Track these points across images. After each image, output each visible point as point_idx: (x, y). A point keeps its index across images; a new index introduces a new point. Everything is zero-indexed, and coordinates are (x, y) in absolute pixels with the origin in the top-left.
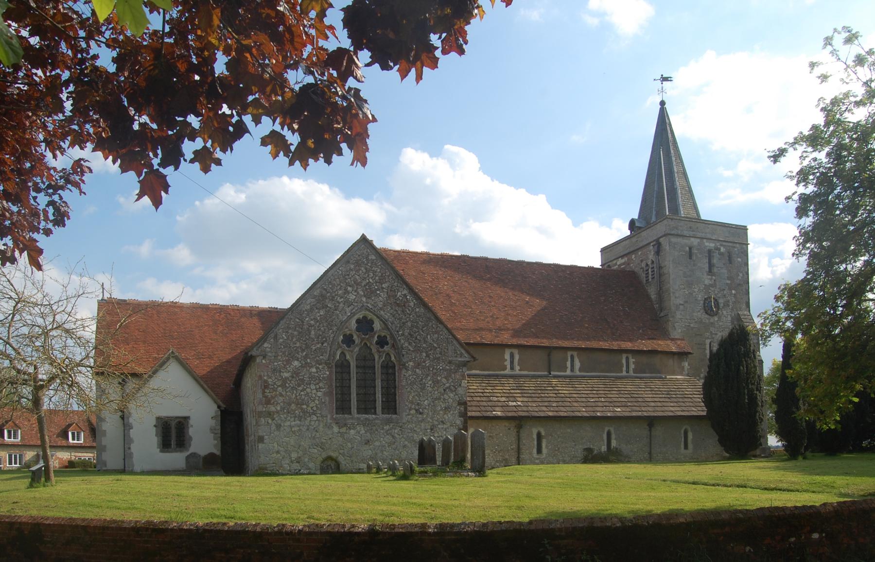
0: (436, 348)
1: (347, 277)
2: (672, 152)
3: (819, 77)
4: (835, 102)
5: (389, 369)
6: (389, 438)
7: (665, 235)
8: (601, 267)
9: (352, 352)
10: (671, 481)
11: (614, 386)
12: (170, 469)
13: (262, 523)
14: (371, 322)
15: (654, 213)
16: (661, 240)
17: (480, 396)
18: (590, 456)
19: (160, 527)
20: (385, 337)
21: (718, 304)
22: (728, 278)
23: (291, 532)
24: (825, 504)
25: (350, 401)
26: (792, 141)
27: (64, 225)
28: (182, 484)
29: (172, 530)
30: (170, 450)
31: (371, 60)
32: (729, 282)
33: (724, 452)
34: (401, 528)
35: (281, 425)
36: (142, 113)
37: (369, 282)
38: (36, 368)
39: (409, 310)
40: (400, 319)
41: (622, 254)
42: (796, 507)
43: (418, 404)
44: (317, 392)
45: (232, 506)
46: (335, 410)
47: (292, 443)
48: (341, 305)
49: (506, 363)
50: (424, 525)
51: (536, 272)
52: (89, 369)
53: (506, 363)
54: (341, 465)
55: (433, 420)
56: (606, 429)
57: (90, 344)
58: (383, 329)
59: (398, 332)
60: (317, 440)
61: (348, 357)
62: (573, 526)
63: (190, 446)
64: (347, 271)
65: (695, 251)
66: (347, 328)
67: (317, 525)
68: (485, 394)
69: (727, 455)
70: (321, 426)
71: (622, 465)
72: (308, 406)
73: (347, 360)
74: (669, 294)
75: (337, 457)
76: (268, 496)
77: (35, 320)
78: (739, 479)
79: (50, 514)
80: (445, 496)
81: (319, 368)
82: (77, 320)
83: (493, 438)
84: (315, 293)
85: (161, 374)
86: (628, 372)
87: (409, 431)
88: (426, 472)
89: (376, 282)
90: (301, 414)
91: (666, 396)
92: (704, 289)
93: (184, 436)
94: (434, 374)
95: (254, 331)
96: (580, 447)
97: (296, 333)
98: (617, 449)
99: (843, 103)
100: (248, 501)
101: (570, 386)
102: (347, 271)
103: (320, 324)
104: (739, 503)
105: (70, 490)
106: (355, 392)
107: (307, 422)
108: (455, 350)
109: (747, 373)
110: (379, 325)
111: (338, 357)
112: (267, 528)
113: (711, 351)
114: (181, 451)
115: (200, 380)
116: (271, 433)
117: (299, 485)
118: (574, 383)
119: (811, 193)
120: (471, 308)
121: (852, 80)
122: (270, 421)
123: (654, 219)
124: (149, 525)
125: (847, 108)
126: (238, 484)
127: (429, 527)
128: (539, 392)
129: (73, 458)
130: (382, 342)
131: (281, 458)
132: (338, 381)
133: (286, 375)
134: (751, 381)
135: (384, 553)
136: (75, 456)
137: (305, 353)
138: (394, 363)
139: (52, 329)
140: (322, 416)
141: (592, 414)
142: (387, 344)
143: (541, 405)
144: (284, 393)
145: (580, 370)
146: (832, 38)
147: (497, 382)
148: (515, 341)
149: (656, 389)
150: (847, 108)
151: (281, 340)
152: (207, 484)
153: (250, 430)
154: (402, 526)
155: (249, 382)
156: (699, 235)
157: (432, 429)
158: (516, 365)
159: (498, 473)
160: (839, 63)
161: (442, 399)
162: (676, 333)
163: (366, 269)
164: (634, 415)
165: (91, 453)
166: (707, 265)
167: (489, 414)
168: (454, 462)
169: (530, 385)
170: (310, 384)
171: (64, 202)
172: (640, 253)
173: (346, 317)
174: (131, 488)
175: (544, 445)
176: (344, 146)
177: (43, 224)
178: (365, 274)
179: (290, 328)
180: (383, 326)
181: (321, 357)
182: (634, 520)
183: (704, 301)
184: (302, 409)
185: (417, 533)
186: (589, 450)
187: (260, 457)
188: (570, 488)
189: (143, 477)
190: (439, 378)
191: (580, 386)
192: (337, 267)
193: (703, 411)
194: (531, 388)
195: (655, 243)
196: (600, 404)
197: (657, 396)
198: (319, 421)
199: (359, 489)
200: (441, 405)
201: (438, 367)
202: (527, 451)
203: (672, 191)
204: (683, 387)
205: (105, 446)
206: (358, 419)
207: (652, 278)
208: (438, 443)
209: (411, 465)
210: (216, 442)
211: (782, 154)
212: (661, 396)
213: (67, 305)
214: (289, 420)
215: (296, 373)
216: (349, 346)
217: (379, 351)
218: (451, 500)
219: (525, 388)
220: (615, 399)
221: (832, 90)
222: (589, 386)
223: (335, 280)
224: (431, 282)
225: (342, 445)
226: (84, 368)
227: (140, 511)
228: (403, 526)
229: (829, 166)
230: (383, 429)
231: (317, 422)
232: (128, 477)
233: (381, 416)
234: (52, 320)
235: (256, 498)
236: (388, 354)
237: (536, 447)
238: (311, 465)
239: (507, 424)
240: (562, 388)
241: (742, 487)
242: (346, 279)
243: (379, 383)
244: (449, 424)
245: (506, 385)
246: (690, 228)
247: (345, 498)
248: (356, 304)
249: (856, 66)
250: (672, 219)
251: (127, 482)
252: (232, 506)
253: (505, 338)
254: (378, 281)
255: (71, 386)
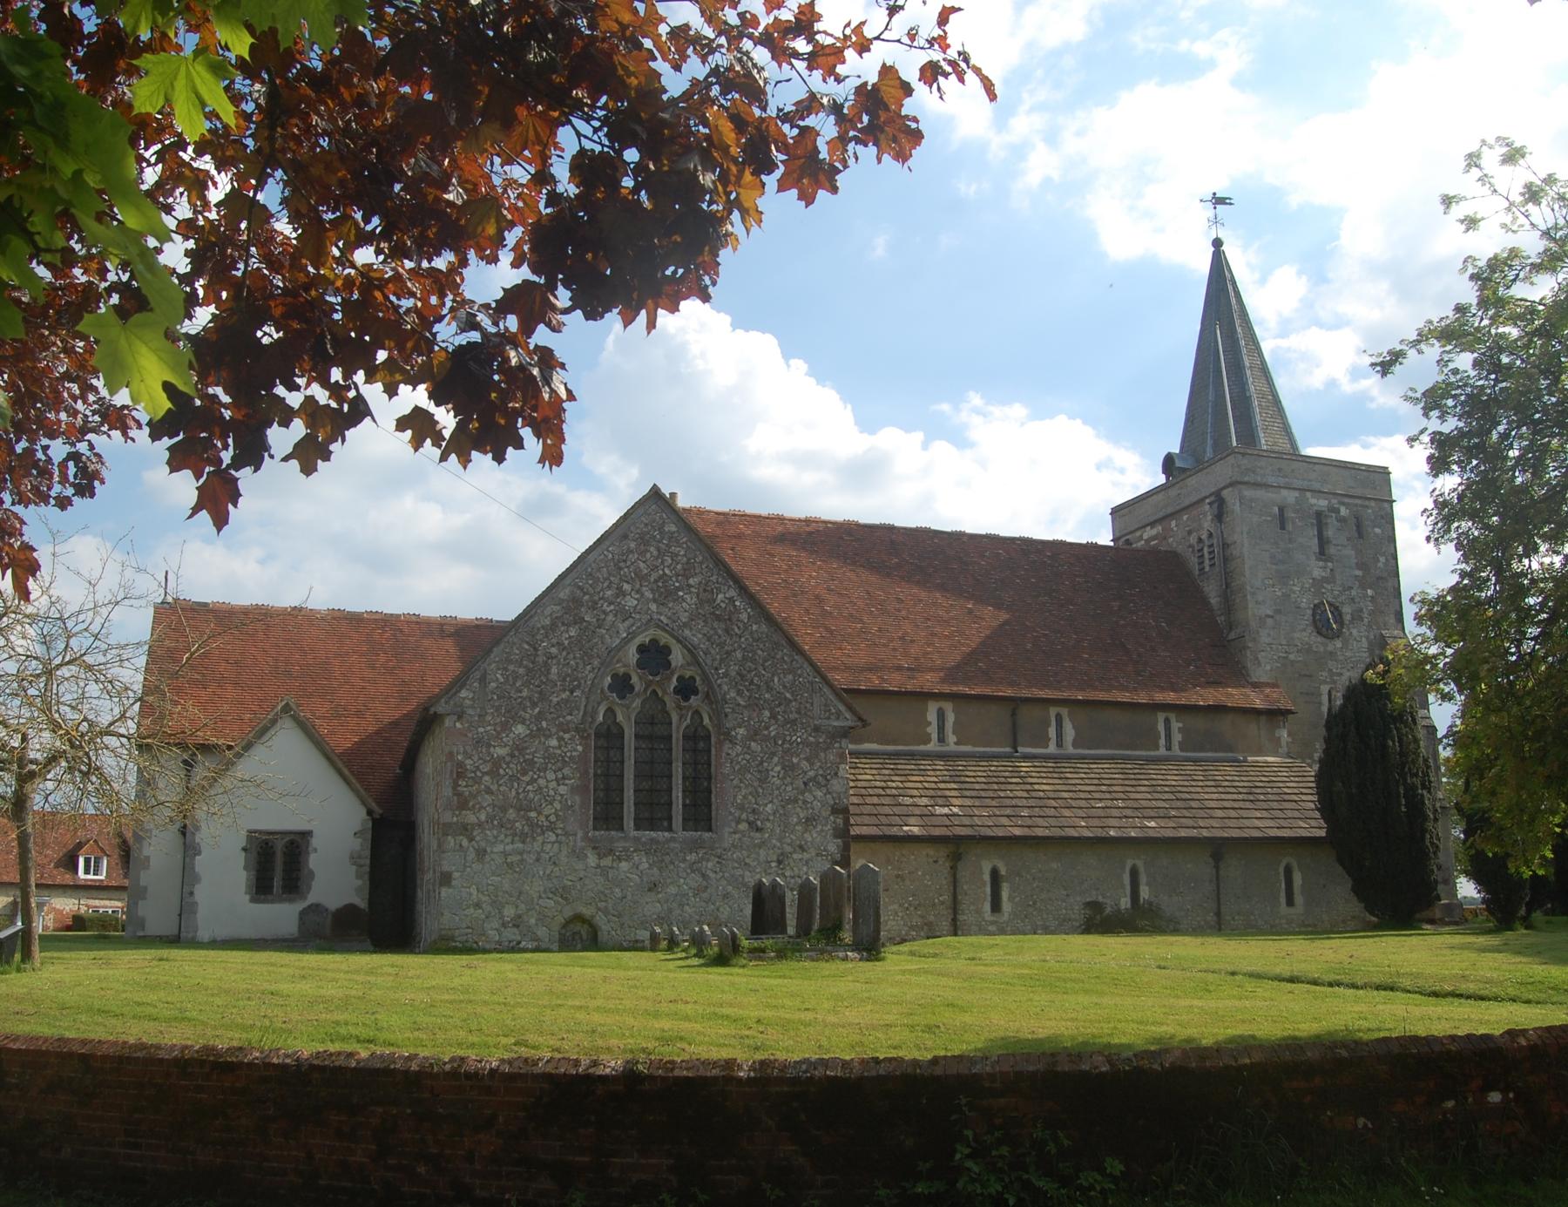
0: (790, 701)
1: (622, 564)
2: (1239, 330)
3: (1462, 221)
4: (1495, 264)
5: (698, 741)
6: (695, 880)
7: (1231, 485)
8: (1112, 544)
9: (628, 708)
10: (1245, 974)
11: (1142, 777)
12: (269, 938)
13: (422, 1055)
14: (666, 651)
15: (1210, 442)
16: (1225, 493)
17: (879, 796)
18: (1098, 917)
19: (229, 1059)
20: (692, 678)
21: (1340, 615)
22: (1360, 566)
23: (476, 1074)
24: (1511, 1034)
25: (623, 803)
26: (1413, 337)
27: (92, 495)
28: (282, 970)
29: (250, 1065)
30: (270, 897)
31: (571, 303)
32: (1359, 573)
33: (1367, 914)
34: (687, 1069)
35: (485, 851)
36: (210, 379)
37: (665, 574)
38: (24, 739)
39: (739, 628)
40: (721, 645)
41: (1152, 519)
42: (1453, 1038)
43: (754, 811)
44: (559, 785)
45: (373, 1018)
46: (591, 823)
47: (507, 886)
48: (610, 618)
49: (929, 730)
50: (730, 1064)
51: (987, 554)
52: (124, 740)
53: (929, 730)
54: (599, 933)
55: (782, 843)
56: (1129, 863)
57: (129, 692)
58: (688, 664)
59: (716, 669)
60: (554, 881)
61: (620, 718)
62: (1017, 1069)
63: (309, 888)
64: (623, 554)
65: (1290, 514)
66: (618, 662)
67: (526, 1060)
68: (888, 791)
69: (1374, 919)
70: (565, 852)
71: (1159, 938)
72: (539, 813)
73: (618, 724)
74: (1245, 596)
75: (593, 917)
76: (447, 997)
77: (31, 648)
78: (1381, 972)
79: (23, 1028)
80: (787, 1002)
81: (563, 739)
82: (110, 647)
83: (903, 880)
84: (561, 595)
85: (259, 753)
86: (1169, 748)
87: (736, 865)
88: (763, 951)
89: (677, 575)
90: (526, 828)
91: (1246, 797)
92: (1313, 585)
93: (299, 870)
94: (786, 752)
95: (445, 662)
96: (1078, 899)
97: (521, 671)
98: (1150, 904)
99: (1510, 267)
100: (404, 1008)
101: (1055, 775)
102: (623, 554)
103: (568, 653)
104: (1365, 1024)
105: (67, 980)
106: (632, 786)
107: (537, 846)
108: (826, 705)
109: (1402, 754)
110: (680, 656)
111: (601, 718)
112: (431, 1064)
113: (1330, 709)
114: (291, 901)
115: (336, 759)
116: (465, 867)
117: (510, 975)
118: (1064, 770)
119: (1452, 431)
120: (861, 621)
121: (1523, 226)
122: (465, 843)
123: (1209, 453)
124: (208, 1056)
125: (1517, 275)
126: (391, 970)
127: (740, 1067)
128: (996, 787)
129: (83, 909)
130: (686, 689)
131: (483, 917)
132: (599, 764)
133: (500, 751)
134: (1410, 769)
135: (651, 1118)
136: (86, 906)
137: (537, 710)
138: (709, 732)
139: (60, 665)
140: (566, 834)
141: (1099, 833)
142: (696, 692)
143: (998, 813)
144: (494, 788)
145: (1075, 744)
146: (1479, 155)
147: (913, 767)
148: (946, 689)
149: (1226, 783)
150: (1517, 275)
151: (493, 685)
152: (333, 971)
153: (426, 859)
154: (688, 1064)
155: (430, 764)
156: (1298, 483)
157: (779, 862)
158: (950, 734)
159: (912, 953)
160: (1495, 197)
161: (800, 802)
162: (1261, 673)
163: (658, 550)
164: (1183, 834)
165: (119, 900)
166: (1316, 540)
167: (894, 831)
168: (819, 931)
169: (976, 773)
170: (545, 770)
171: (97, 455)
172: (1185, 517)
173: (618, 641)
174: (186, 977)
175: (1005, 894)
176: (526, 433)
177: (57, 489)
178: (657, 558)
179: (510, 662)
180: (689, 658)
181: (569, 718)
182: (1134, 1060)
183: (1314, 610)
184: (528, 819)
185: (715, 1078)
186: (1095, 906)
187: (442, 914)
188: (1043, 986)
189: (212, 953)
190: (795, 760)
191: (1076, 776)
192: (604, 546)
193: (1320, 828)
194: (979, 779)
195: (1212, 498)
196: (1115, 813)
197: (1230, 796)
198: (560, 843)
199: (623, 985)
200: (798, 814)
201: (794, 738)
202: (972, 908)
203: (1236, 368)
204: (1279, 779)
205: (145, 888)
206: (637, 839)
207: (1211, 566)
208: (792, 890)
209: (734, 936)
210: (359, 882)
211: (1396, 360)
212: (1235, 796)
213: (93, 619)
214: (502, 841)
215: (519, 748)
216: (622, 697)
217: (679, 707)
218: (799, 1010)
219: (968, 779)
220: (1144, 803)
221: (1487, 244)
222: (1093, 776)
223: (599, 570)
224: (786, 571)
225: (602, 893)
226: (115, 738)
227: (195, 1026)
228: (690, 1065)
229: (1480, 383)
230: (684, 860)
231: (556, 845)
232: (183, 952)
233: (682, 835)
234: (63, 646)
235: (422, 1002)
236: (697, 713)
237: (989, 898)
238: (542, 932)
239: (932, 853)
240: (1040, 781)
241: (1385, 989)
242: (621, 569)
243: (678, 770)
244: (813, 852)
245: (929, 773)
246: (1280, 470)
247: (593, 1004)
248: (638, 616)
249: (1527, 203)
250: (1244, 454)
251: (177, 964)
252: (373, 1018)
253: (929, 681)
254: (682, 572)
255: (85, 775)
